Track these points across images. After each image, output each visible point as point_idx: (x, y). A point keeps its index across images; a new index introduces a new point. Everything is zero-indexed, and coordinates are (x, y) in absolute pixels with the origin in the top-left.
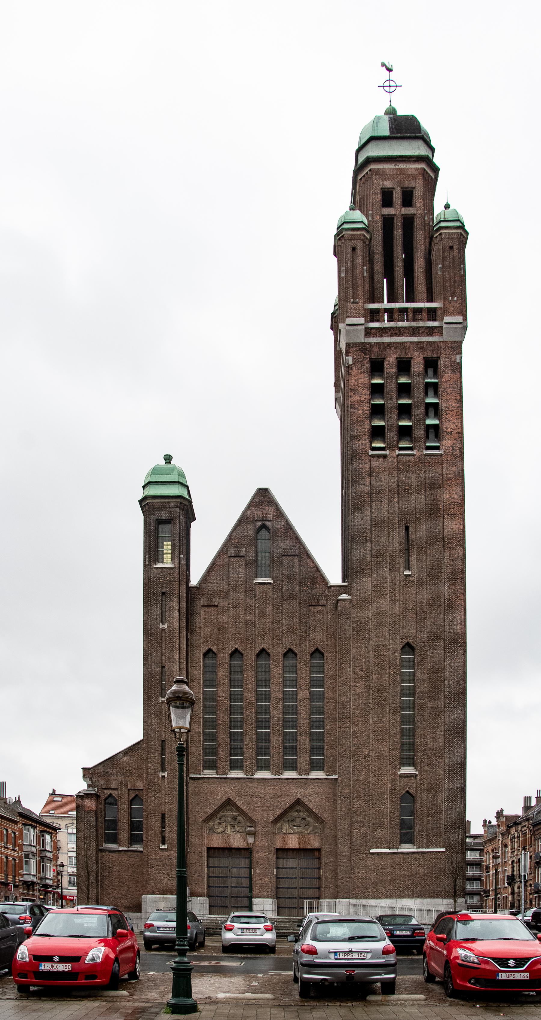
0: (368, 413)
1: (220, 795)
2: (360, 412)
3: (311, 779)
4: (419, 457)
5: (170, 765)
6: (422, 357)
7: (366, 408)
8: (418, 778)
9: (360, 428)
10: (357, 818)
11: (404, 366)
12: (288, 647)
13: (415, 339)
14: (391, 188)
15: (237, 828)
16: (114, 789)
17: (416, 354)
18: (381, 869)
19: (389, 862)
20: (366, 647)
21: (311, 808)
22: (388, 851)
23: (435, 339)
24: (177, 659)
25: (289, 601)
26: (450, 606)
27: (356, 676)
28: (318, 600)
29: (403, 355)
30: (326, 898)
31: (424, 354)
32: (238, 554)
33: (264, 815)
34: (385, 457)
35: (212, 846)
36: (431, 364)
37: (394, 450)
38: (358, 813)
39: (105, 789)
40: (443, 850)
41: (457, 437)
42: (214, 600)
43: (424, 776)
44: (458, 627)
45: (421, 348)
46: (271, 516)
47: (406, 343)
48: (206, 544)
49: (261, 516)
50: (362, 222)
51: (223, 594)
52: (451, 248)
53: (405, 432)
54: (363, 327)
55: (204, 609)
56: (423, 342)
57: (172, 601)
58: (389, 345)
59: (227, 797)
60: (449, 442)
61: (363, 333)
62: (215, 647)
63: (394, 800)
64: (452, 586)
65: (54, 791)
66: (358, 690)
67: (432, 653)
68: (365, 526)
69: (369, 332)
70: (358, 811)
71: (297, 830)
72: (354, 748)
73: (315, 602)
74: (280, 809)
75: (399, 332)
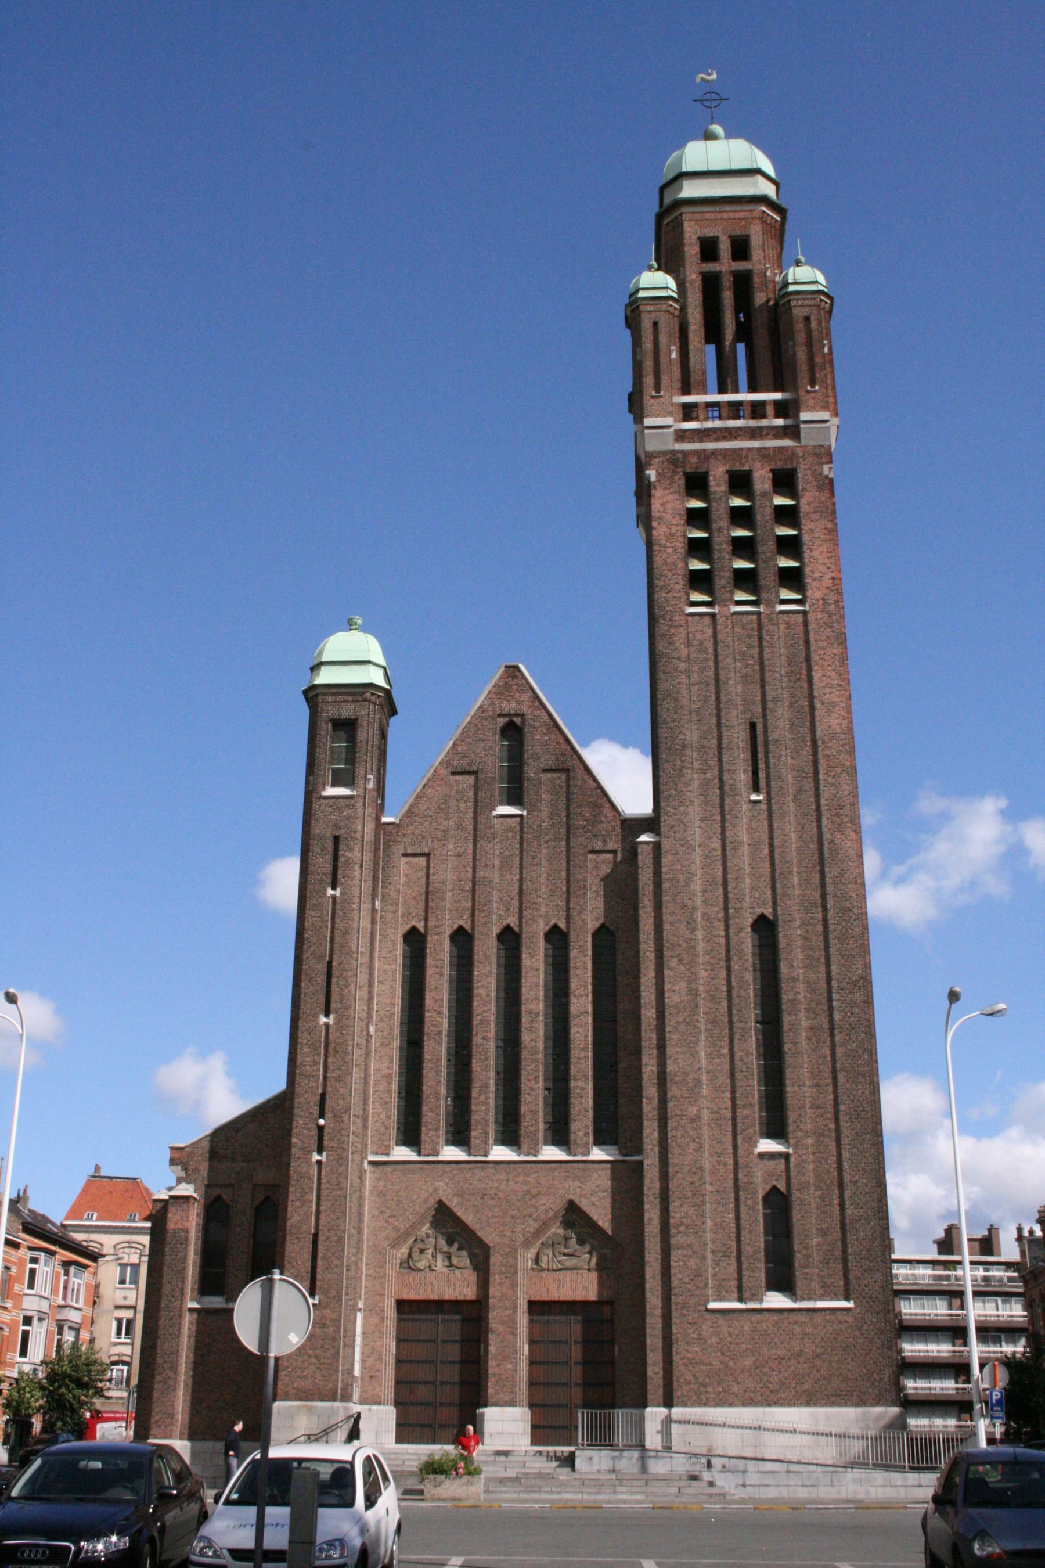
0: (682, 551)
1: (424, 1195)
2: (670, 550)
5: (331, 1139)
6: (768, 469)
7: (679, 545)
9: (670, 574)
11: (740, 482)
12: (553, 922)
13: (756, 444)
16: (226, 1186)
17: (757, 465)
18: (731, 1343)
19: (746, 1328)
24: (354, 949)
25: (554, 844)
28: (604, 842)
29: (737, 467)
30: (624, 1406)
32: (467, 768)
37: (726, 606)
38: (682, 1228)
40: (850, 1305)
41: (830, 585)
42: (423, 844)
43: (804, 1157)
44: (850, 886)
46: (525, 709)
47: (741, 449)
49: (507, 708)
51: (440, 835)
55: (404, 860)
57: (351, 850)
58: (715, 453)
59: (437, 1198)
61: (672, 437)
64: (836, 819)
65: (97, 1168)
67: (807, 931)
68: (682, 723)
69: (682, 436)
70: (682, 1224)
73: (599, 846)
74: (535, 1220)
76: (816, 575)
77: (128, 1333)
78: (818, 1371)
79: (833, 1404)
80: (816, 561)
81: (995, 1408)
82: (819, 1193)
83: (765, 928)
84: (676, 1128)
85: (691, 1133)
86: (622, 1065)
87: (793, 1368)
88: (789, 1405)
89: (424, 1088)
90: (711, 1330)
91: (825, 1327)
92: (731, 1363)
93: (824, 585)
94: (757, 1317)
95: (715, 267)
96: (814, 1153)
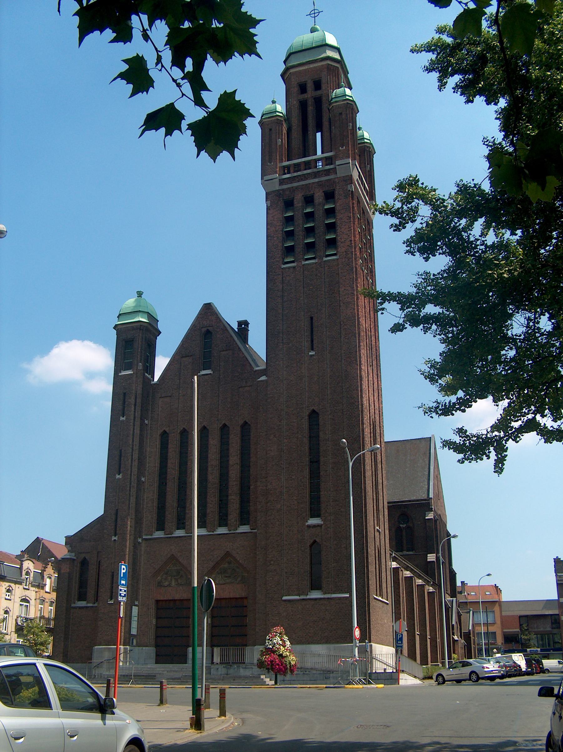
3: (238, 533)
6: (321, 191)
8: (323, 527)
11: (309, 200)
12: (223, 422)
13: (316, 180)
15: (179, 581)
18: (292, 615)
22: (297, 597)
23: (332, 177)
35: (159, 599)
36: (330, 196)
39: (81, 553)
43: (328, 526)
45: (320, 185)
47: (309, 184)
52: (341, 114)
53: (310, 247)
54: (277, 180)
55: (161, 400)
58: (297, 187)
69: (282, 182)
71: (228, 581)
72: (269, 504)
75: (305, 177)
77: (434, 660)
79: (338, 642)
80: (342, 234)
82: (335, 542)
83: (314, 415)
86: (252, 487)
87: (320, 626)
88: (318, 643)
89: (167, 504)
92: (292, 625)
95: (305, 96)
96: (333, 523)
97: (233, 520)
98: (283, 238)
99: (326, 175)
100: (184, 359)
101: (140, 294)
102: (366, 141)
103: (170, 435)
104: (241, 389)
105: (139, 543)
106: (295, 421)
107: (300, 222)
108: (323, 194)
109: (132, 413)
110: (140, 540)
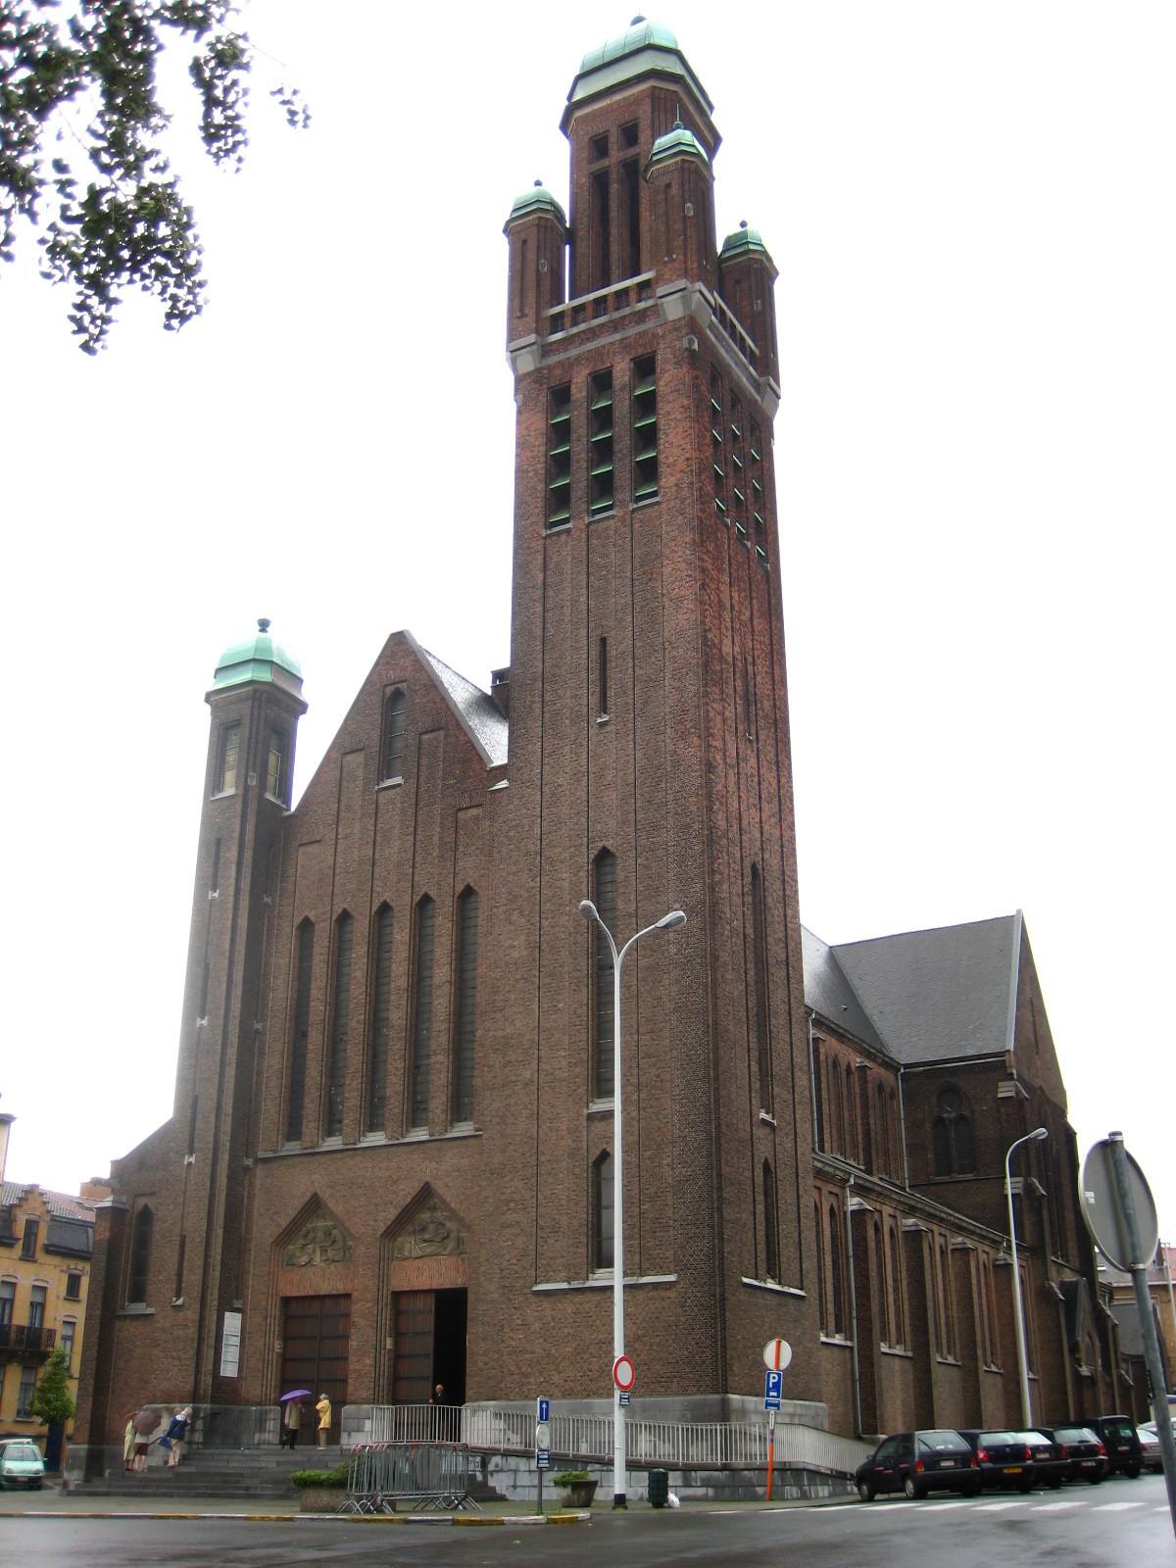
4: (623, 517)
6: (627, 359)
10: (510, 1217)
11: (602, 382)
13: (617, 337)
14: (605, 132)
18: (554, 1328)
20: (530, 870)
21: (448, 1200)
22: (565, 1286)
26: (676, 764)
27: (513, 928)
28: (471, 797)
29: (600, 366)
31: (631, 354)
33: (369, 1219)
34: (568, 531)
35: (288, 1295)
48: (313, 742)
50: (694, 146)
52: (668, 186)
56: (630, 337)
60: (672, 479)
62: (313, 913)
63: (577, 1171)
66: (516, 954)
71: (428, 1250)
75: (592, 334)
76: (671, 460)
78: (638, 1355)
81: (771, 1394)
84: (510, 1096)
85: (525, 1100)
89: (307, 1079)
90: (536, 1314)
91: (647, 1305)
93: (678, 468)
94: (578, 1298)
95: (605, 162)
97: (438, 1111)
98: (547, 471)
99: (637, 323)
100: (349, 758)
101: (264, 625)
102: (751, 247)
103: (317, 927)
104: (461, 815)
105: (246, 1169)
106: (564, 876)
107: (583, 431)
108: (632, 365)
109: (233, 881)
110: (249, 1162)
